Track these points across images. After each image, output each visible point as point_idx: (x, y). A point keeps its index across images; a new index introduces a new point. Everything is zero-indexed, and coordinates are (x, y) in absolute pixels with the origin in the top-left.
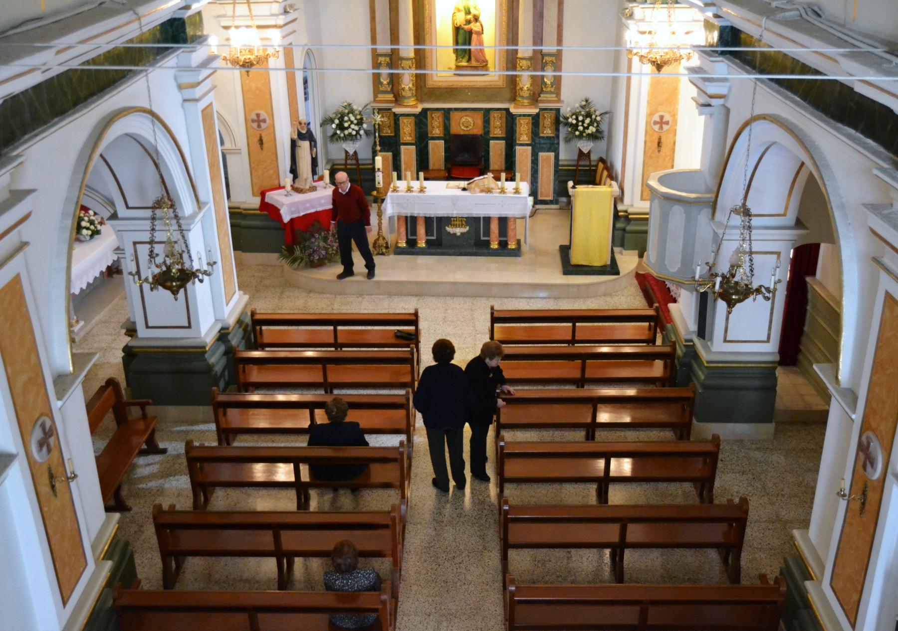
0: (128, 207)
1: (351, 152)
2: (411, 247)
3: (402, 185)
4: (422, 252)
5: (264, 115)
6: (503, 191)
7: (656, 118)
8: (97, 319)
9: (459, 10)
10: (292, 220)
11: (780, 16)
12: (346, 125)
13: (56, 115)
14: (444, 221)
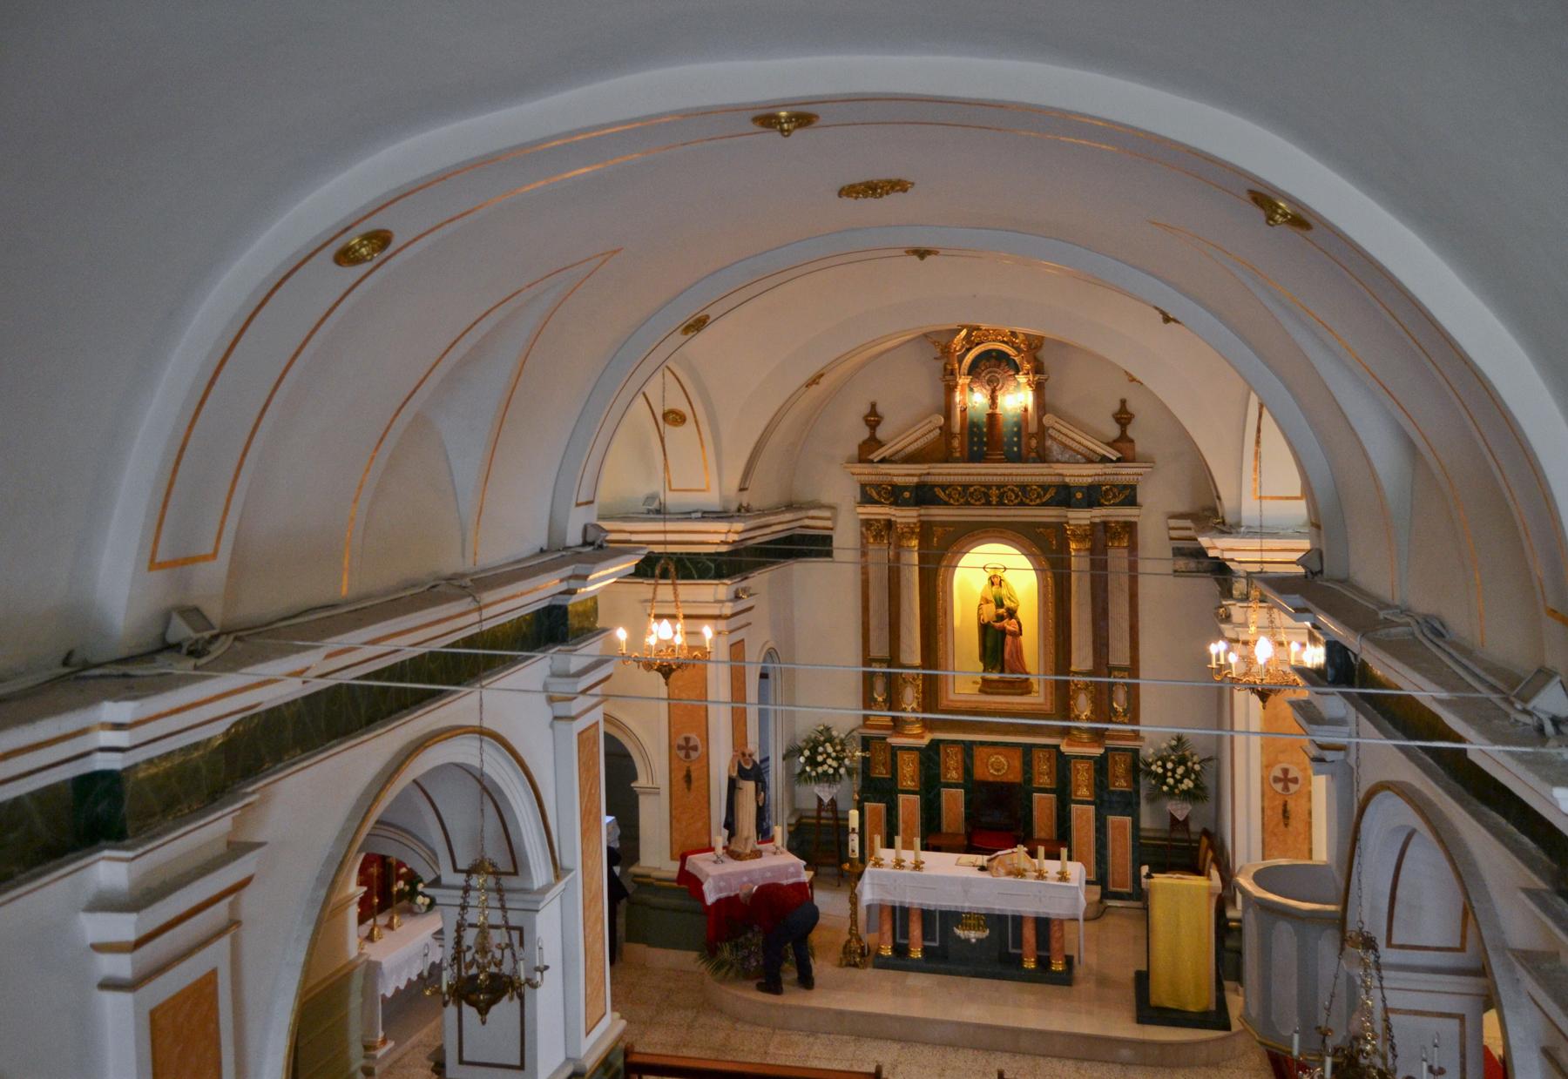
0: (456, 870)
1: (826, 800)
2: (900, 959)
3: (887, 855)
4: (917, 967)
5: (695, 740)
6: (1041, 875)
7: (1277, 772)
8: (414, 1039)
9: (987, 602)
10: (719, 901)
11: (1382, 633)
12: (820, 759)
13: (335, 737)
14: (952, 918)
